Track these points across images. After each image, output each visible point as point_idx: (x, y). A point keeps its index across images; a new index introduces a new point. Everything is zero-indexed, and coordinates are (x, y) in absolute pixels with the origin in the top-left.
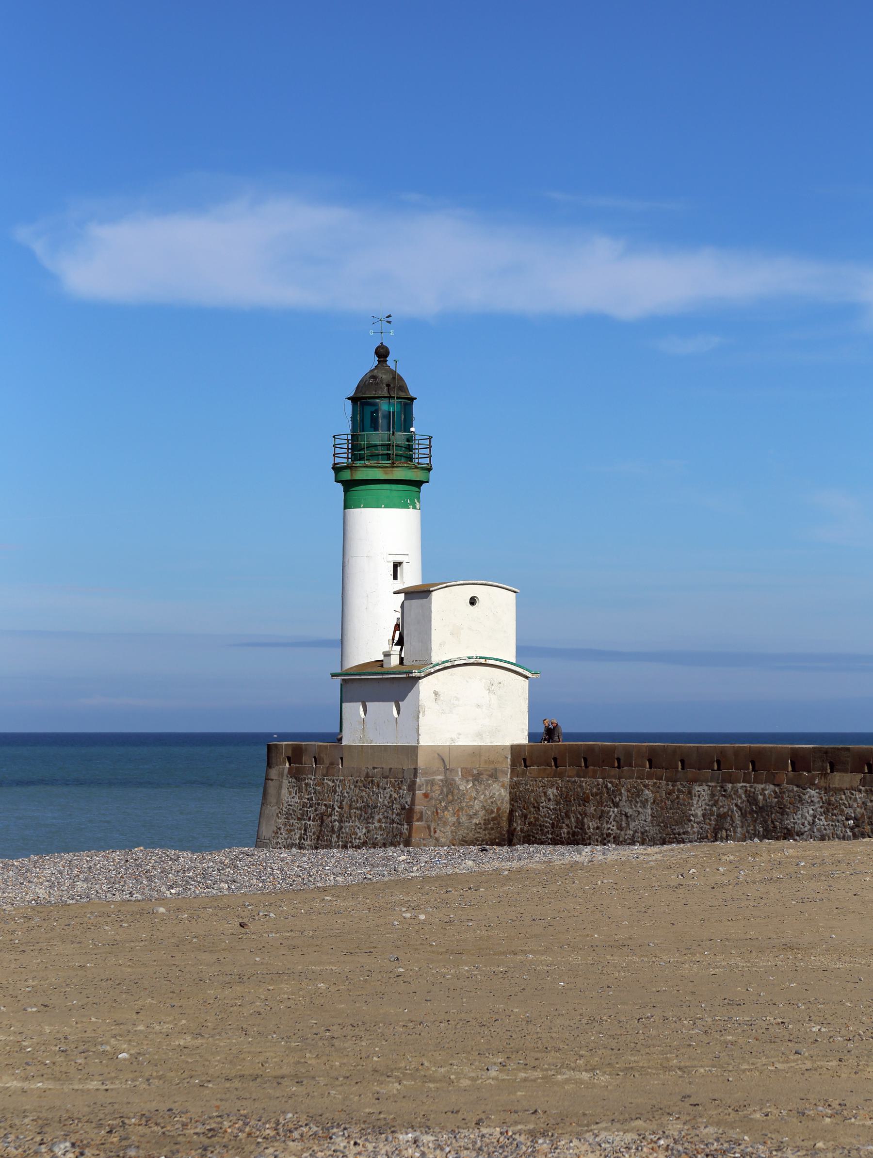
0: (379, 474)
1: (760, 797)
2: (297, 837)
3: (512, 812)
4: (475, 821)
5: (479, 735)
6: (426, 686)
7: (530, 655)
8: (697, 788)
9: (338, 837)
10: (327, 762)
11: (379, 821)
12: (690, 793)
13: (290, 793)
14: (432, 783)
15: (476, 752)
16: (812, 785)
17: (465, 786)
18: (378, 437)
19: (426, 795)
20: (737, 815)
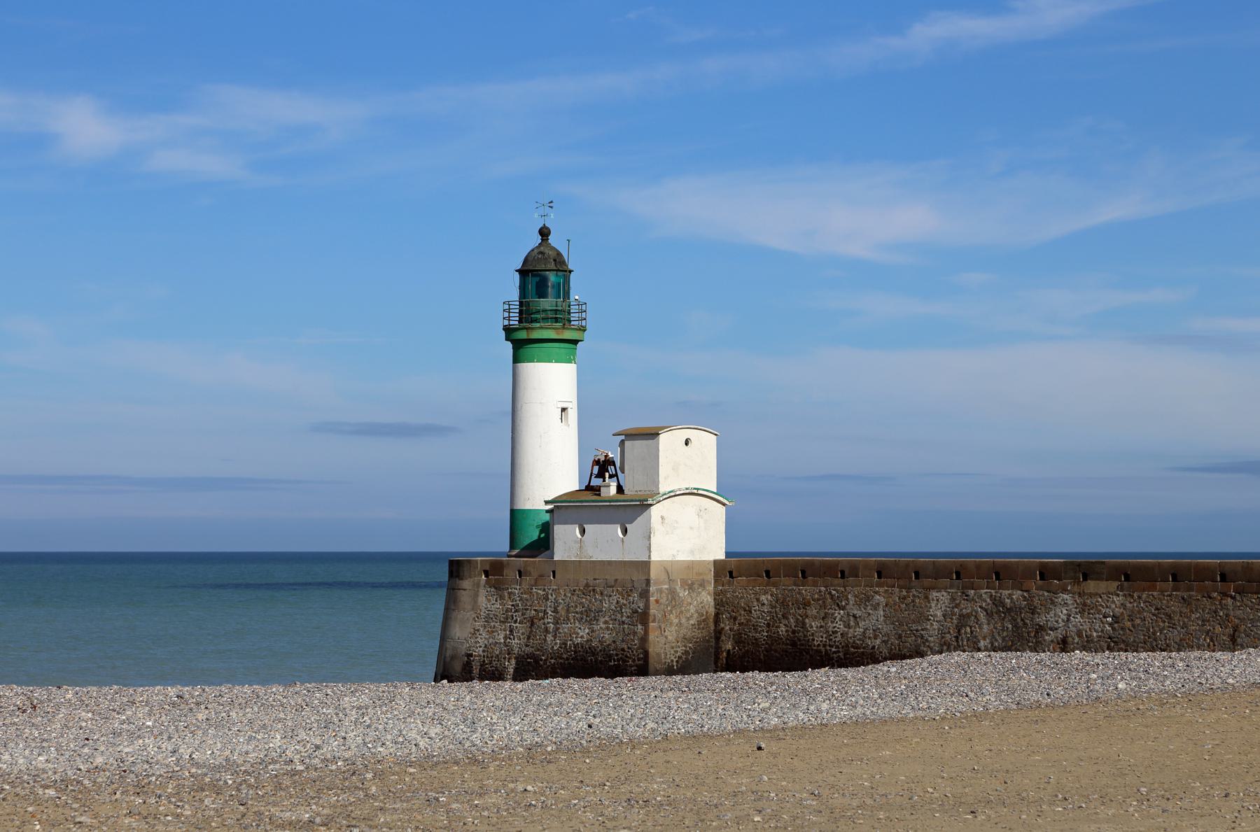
0: (551, 334)
1: (1008, 601)
2: (502, 636)
3: (717, 615)
4: (692, 622)
5: (692, 552)
6: (656, 511)
7: (730, 488)
8: (934, 594)
9: (555, 636)
10: (535, 575)
11: (606, 622)
12: (927, 597)
13: (489, 601)
14: (660, 591)
15: (691, 566)
16: (1065, 590)
17: (683, 594)
18: (547, 303)
19: (657, 601)
20: (982, 616)
